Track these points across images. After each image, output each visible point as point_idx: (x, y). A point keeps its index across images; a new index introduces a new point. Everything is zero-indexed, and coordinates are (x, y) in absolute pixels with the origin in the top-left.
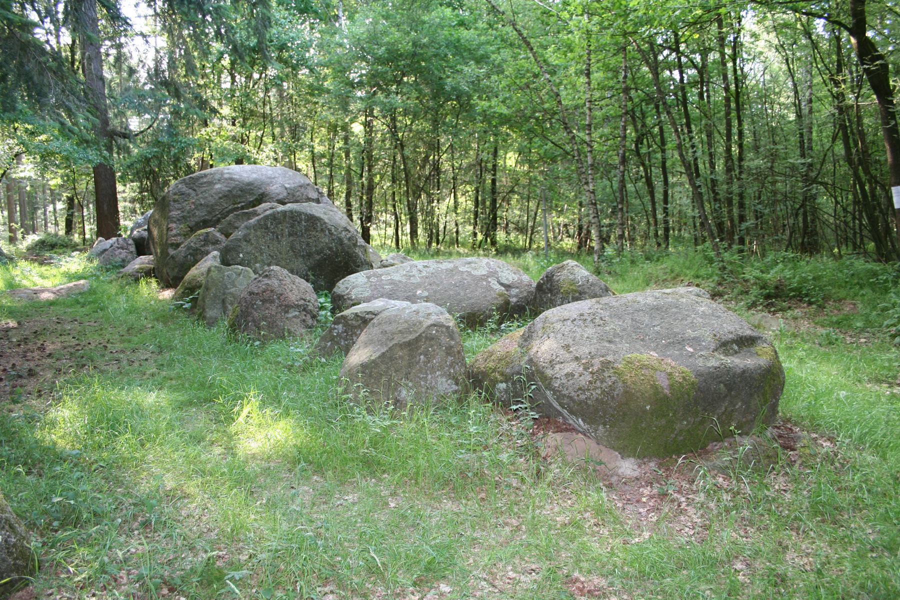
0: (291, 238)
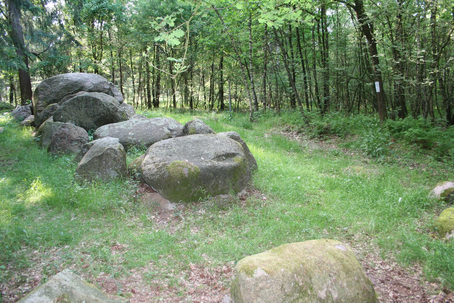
0: (86, 109)
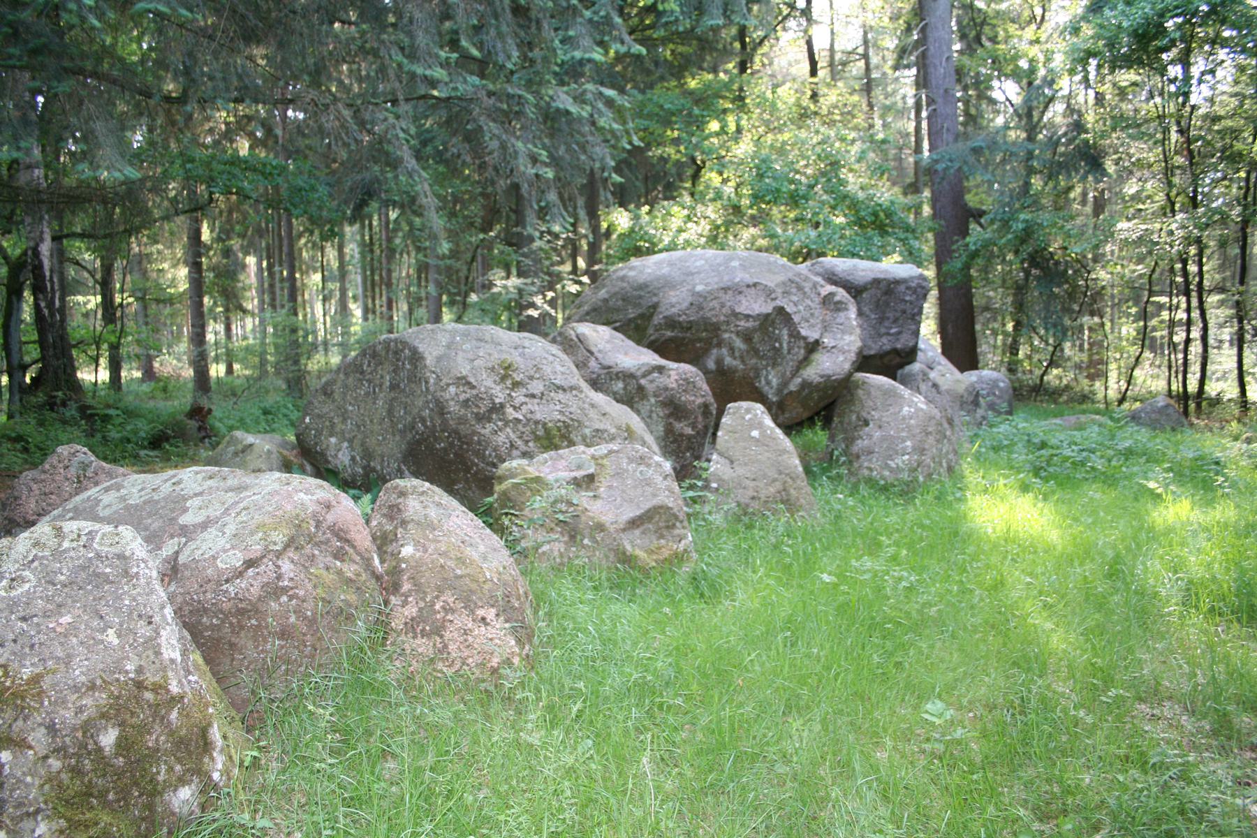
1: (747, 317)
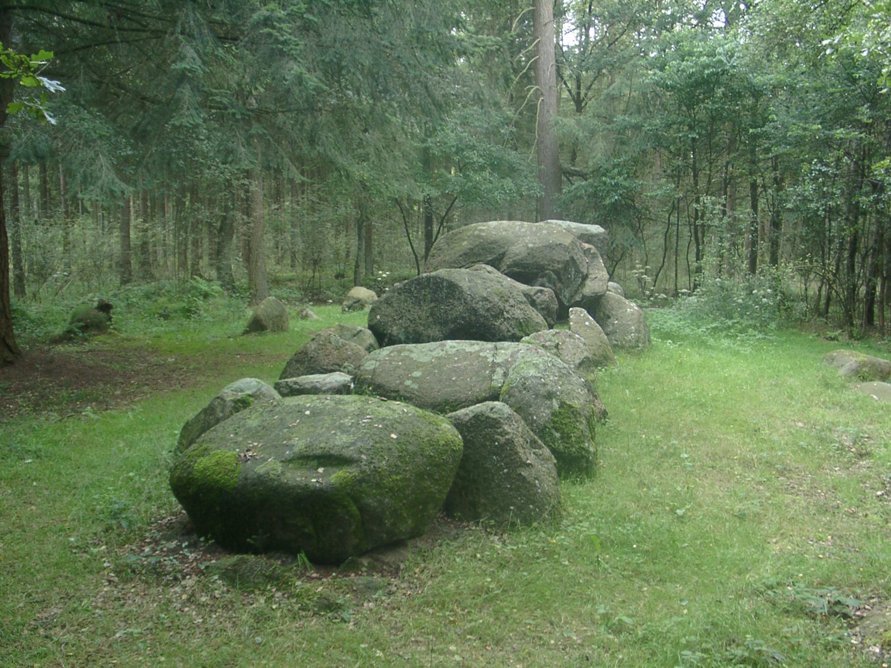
0: (433, 305)
1: (558, 262)
